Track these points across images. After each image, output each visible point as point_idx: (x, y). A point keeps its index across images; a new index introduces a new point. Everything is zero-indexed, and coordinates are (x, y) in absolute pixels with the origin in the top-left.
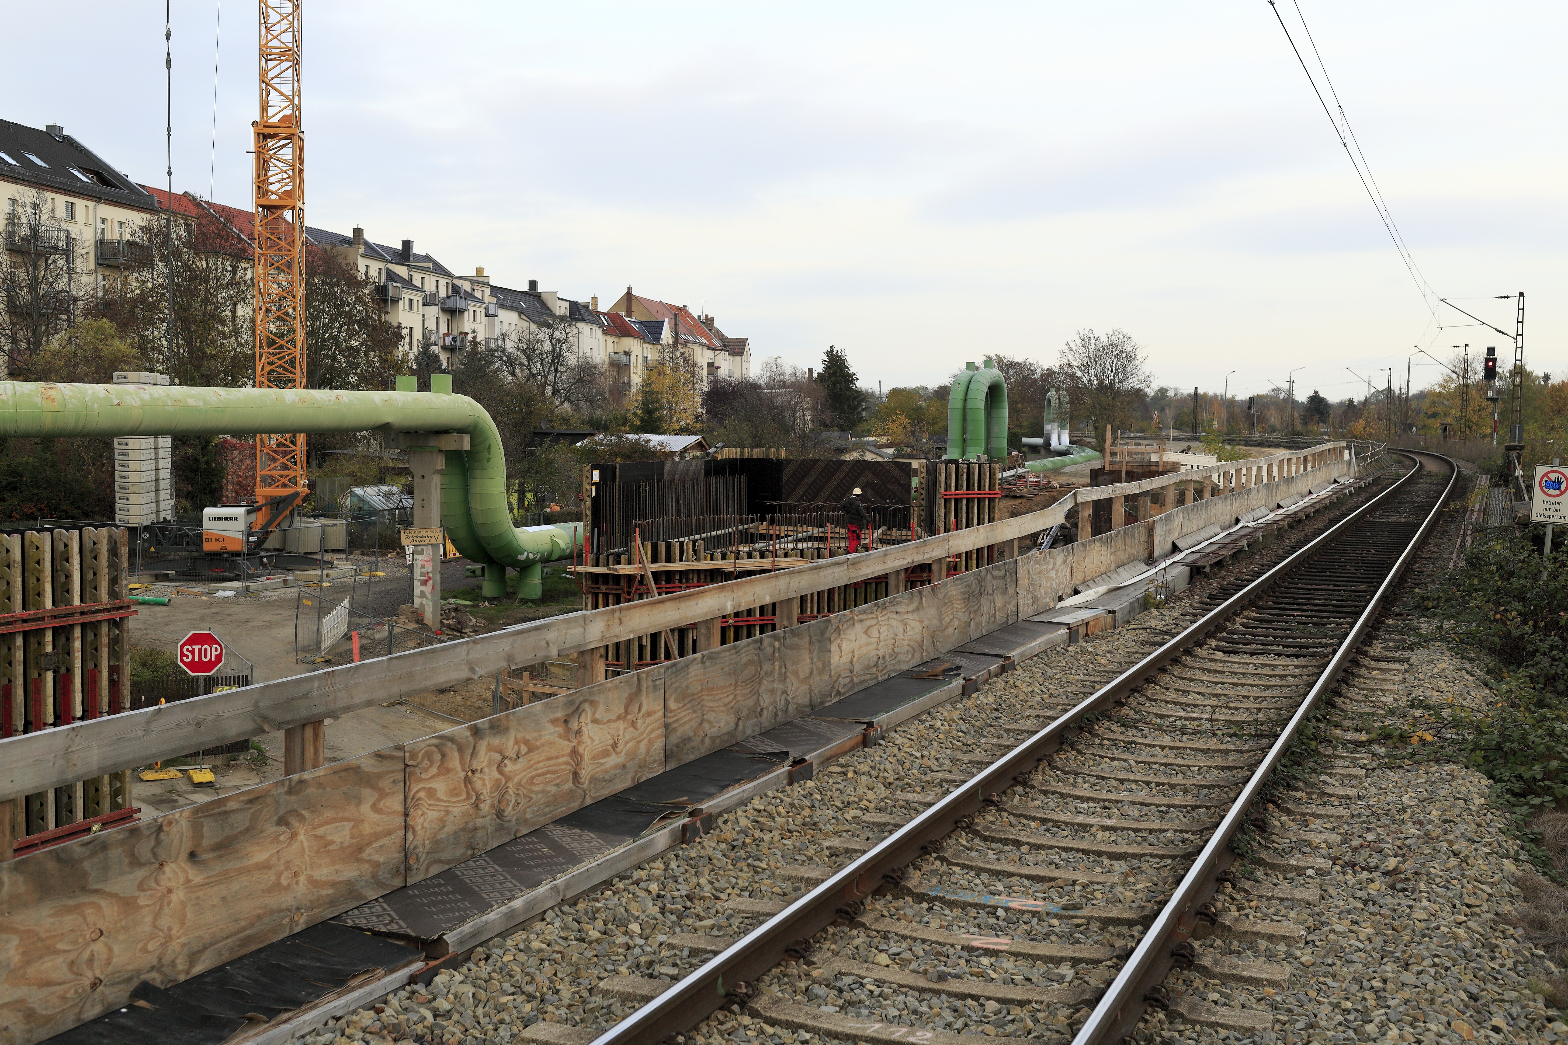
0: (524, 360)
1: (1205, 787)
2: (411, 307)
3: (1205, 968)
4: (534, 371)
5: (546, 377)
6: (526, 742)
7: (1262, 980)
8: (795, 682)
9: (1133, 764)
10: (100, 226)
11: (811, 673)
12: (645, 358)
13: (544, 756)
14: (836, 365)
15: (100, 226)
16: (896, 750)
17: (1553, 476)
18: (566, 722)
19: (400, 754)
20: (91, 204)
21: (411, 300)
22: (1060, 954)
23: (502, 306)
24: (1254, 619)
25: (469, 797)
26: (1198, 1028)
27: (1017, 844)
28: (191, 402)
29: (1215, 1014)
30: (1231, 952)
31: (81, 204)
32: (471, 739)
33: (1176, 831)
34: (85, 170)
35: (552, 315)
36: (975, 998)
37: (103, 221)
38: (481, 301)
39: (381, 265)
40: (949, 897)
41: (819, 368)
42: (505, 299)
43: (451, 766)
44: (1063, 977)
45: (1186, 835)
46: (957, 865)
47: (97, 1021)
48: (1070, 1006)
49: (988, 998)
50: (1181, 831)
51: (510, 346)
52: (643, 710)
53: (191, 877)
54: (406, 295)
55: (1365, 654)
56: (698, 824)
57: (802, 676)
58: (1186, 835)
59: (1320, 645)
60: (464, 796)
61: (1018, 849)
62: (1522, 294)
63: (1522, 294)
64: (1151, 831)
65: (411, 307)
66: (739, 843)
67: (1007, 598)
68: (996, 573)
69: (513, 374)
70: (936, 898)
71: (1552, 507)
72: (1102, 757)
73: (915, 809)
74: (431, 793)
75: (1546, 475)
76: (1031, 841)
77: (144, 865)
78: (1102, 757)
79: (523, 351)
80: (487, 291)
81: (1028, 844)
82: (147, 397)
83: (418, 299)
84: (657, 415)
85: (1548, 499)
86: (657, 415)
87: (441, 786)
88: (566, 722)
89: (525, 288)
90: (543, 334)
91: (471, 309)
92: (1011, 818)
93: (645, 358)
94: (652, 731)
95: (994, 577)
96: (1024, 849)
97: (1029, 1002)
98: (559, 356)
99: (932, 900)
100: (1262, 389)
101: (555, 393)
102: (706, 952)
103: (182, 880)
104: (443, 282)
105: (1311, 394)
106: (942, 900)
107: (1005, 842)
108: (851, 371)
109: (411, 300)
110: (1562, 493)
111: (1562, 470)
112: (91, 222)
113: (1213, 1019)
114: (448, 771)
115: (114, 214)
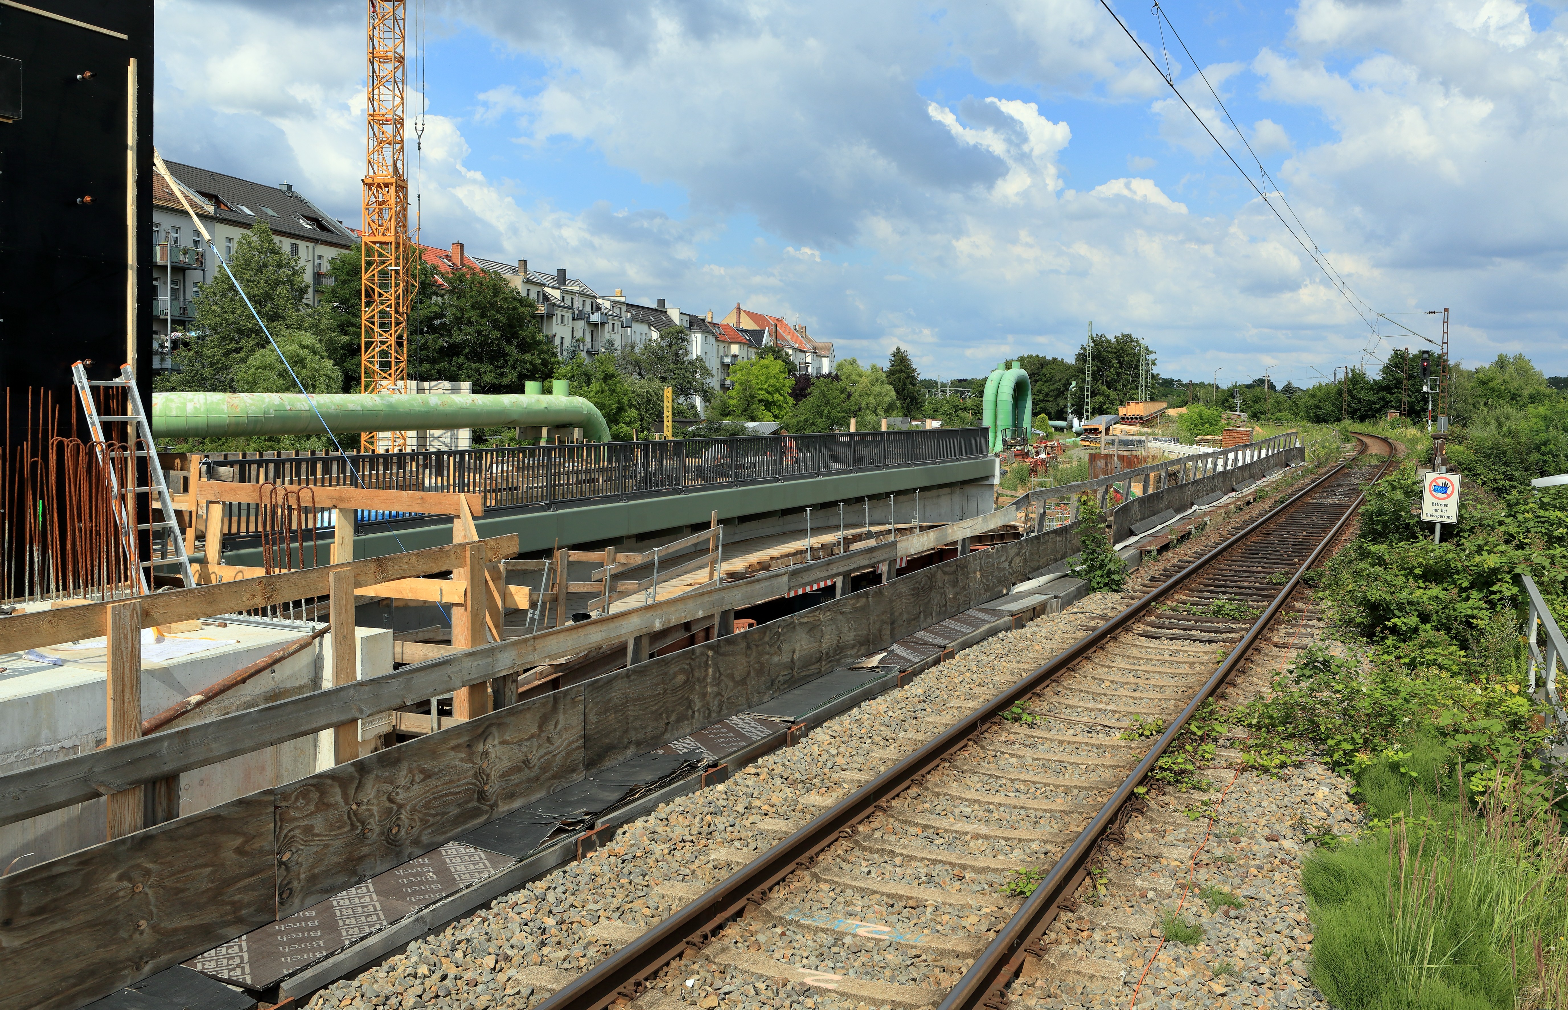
2: (562, 322)
6: (422, 771)
8: (731, 684)
9: (1030, 760)
10: (317, 261)
11: (749, 674)
13: (443, 780)
14: (901, 362)
15: (317, 261)
17: (1440, 482)
19: (272, 798)
20: (311, 245)
21: (562, 316)
22: (882, 997)
23: (636, 320)
25: (353, 827)
27: (892, 854)
28: (351, 407)
31: (302, 245)
32: (356, 774)
34: (309, 218)
37: (320, 257)
41: (886, 365)
42: (638, 314)
43: (332, 801)
45: (1049, 847)
46: (826, 881)
52: (559, 727)
55: (1268, 640)
56: (594, 838)
57: (737, 677)
58: (1049, 847)
59: (1232, 630)
60: (348, 828)
62: (1446, 310)
63: (1446, 310)
64: (1020, 840)
65: (562, 322)
66: (629, 856)
67: (957, 589)
68: (947, 569)
70: (792, 922)
71: (1440, 508)
72: (1003, 753)
74: (308, 830)
75: (1434, 480)
76: (905, 852)
78: (1003, 753)
80: (624, 308)
81: (902, 855)
82: (314, 403)
83: (568, 315)
85: (1436, 501)
87: (319, 824)
88: (469, 746)
91: (610, 322)
94: (572, 742)
95: (945, 573)
96: (898, 860)
100: (1230, 385)
104: (588, 302)
105: (1286, 383)
108: (914, 367)
109: (562, 316)
110: (1449, 496)
112: (311, 258)
114: (329, 806)
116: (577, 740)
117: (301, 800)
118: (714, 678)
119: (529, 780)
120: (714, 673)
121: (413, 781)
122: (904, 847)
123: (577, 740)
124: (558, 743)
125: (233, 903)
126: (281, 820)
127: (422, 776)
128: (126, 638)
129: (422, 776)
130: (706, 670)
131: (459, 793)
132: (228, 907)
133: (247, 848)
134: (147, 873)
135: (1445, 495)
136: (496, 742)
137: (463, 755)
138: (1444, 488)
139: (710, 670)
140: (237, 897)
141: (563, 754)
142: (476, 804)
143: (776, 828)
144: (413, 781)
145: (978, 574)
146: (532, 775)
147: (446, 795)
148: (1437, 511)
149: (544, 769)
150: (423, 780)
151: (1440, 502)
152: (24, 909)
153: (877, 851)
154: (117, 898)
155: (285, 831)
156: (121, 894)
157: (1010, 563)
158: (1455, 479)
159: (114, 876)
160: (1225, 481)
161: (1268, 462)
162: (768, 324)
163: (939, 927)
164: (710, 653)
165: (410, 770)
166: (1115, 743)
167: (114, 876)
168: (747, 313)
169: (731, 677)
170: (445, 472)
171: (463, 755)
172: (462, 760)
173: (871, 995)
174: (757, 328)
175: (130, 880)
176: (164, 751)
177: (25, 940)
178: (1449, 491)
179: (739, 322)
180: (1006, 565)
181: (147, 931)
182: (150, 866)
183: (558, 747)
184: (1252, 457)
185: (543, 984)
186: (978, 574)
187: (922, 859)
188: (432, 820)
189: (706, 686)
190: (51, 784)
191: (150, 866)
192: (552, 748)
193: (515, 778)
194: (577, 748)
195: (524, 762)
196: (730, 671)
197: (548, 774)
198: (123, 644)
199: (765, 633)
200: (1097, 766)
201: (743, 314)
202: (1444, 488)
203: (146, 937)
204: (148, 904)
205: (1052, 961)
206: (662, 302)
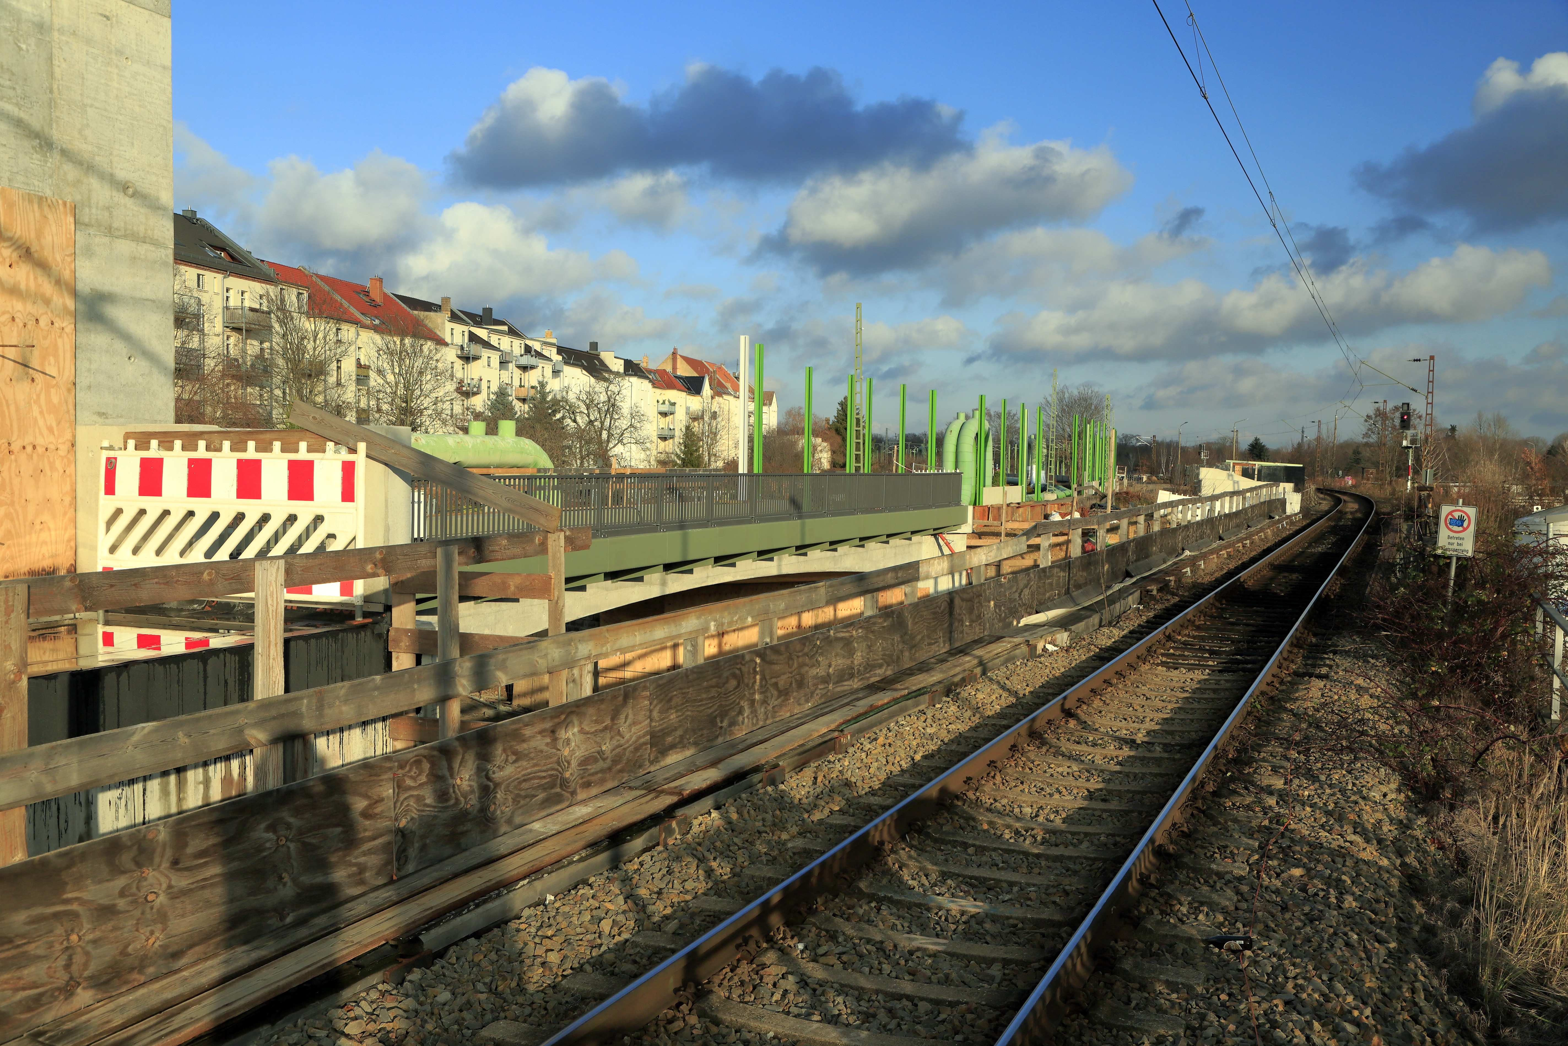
0: (583, 408)
1: (1138, 792)
3: (1125, 971)
4: (592, 418)
5: (602, 423)
7: (1177, 983)
8: (775, 693)
10: (226, 294)
12: (688, 408)
16: (864, 755)
17: (1456, 515)
18: (553, 732)
22: (993, 955)
23: (567, 363)
24: (1194, 637)
26: (1115, 1031)
27: (965, 846)
29: (1131, 1018)
30: (1152, 955)
33: (1108, 835)
35: (609, 371)
36: (909, 998)
38: (549, 359)
39: (466, 328)
40: (896, 897)
44: (993, 978)
45: (1118, 839)
47: (1200, 524)
48: (995, 1008)
49: (922, 999)
50: (1113, 835)
51: (572, 397)
53: (173, 883)
54: (485, 353)
58: (1118, 839)
61: (966, 850)
62: (1432, 358)
63: (1432, 358)
69: (575, 421)
70: (885, 898)
71: (1455, 541)
73: (875, 811)
75: (1450, 513)
76: (977, 843)
77: (124, 872)
79: (584, 402)
81: (974, 845)
84: (696, 454)
85: (1452, 534)
86: (696, 454)
89: (586, 348)
90: (600, 387)
91: (541, 366)
92: (962, 821)
93: (688, 408)
94: (639, 737)
97: (958, 1003)
98: (613, 405)
99: (880, 900)
101: (610, 435)
102: (665, 949)
103: (164, 886)
106: (890, 901)
107: (954, 844)
110: (1465, 529)
111: (1465, 509)
113: (1129, 1023)
115: (237, 284)
116: (644, 736)
117: (414, 770)
118: (761, 686)
119: (602, 771)
120: (761, 680)
121: (507, 760)
122: (975, 839)
123: (644, 736)
124: (627, 736)
125: (357, 865)
126: (399, 787)
127: (514, 757)
128: (272, 596)
129: (514, 757)
130: (755, 677)
131: (544, 777)
132: (354, 869)
133: (370, 812)
134: (289, 826)
135: (1461, 529)
136: (576, 730)
137: (548, 740)
138: (1460, 522)
139: (758, 677)
140: (362, 859)
141: (631, 748)
142: (558, 790)
143: (845, 822)
144: (507, 760)
145: (992, 603)
146: (605, 766)
147: (531, 779)
148: (1452, 544)
149: (615, 762)
150: (515, 761)
151: (1457, 535)
152: (189, 850)
153: (949, 842)
154: (264, 850)
155: (401, 799)
156: (268, 845)
157: (1020, 594)
158: (1472, 511)
159: (263, 826)
160: (1212, 529)
161: (1253, 512)
162: (708, 371)
163: (1029, 903)
164: (758, 660)
165: (504, 751)
166: (1157, 755)
167: (263, 826)
168: (685, 358)
169: (776, 685)
170: (308, 547)
171: (548, 740)
172: (547, 744)
173: (982, 954)
174: (696, 375)
175: (275, 832)
176: (304, 709)
177: (190, 881)
178: (1465, 524)
179: (674, 368)
180: (1016, 596)
181: (289, 884)
182: (292, 820)
183: (628, 741)
184: (1238, 505)
185: (662, 944)
186: (992, 603)
187: (995, 850)
188: (522, 802)
189: (754, 693)
190: (212, 732)
191: (292, 820)
192: (622, 741)
193: (592, 768)
194: (645, 744)
195: (598, 753)
196: (774, 680)
197: (619, 767)
198: (270, 602)
199: (804, 645)
200: (1144, 774)
201: (679, 361)
202: (1460, 522)
203: (287, 891)
204: (289, 858)
205: (1149, 926)
206: (594, 346)
